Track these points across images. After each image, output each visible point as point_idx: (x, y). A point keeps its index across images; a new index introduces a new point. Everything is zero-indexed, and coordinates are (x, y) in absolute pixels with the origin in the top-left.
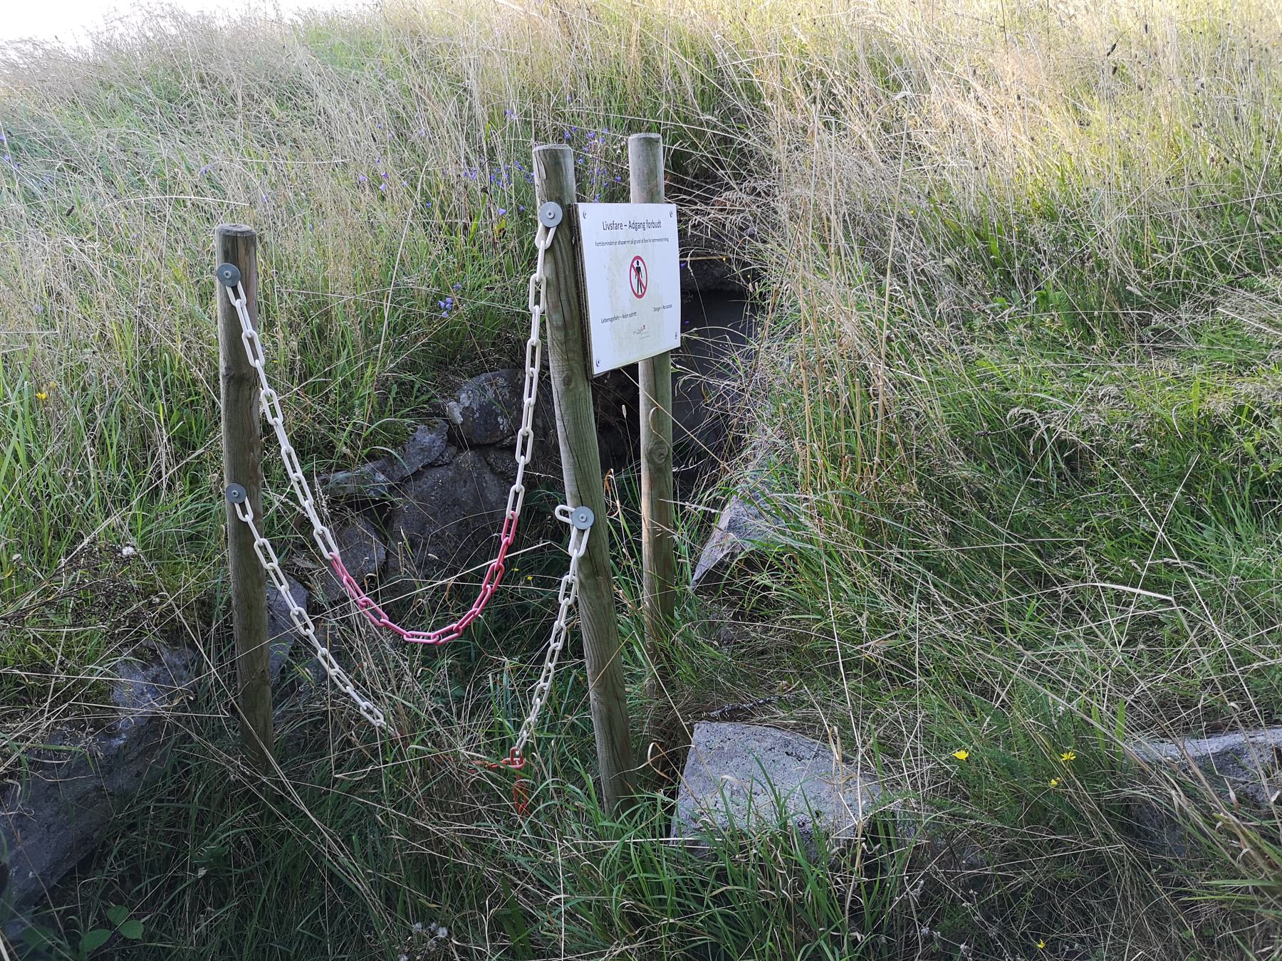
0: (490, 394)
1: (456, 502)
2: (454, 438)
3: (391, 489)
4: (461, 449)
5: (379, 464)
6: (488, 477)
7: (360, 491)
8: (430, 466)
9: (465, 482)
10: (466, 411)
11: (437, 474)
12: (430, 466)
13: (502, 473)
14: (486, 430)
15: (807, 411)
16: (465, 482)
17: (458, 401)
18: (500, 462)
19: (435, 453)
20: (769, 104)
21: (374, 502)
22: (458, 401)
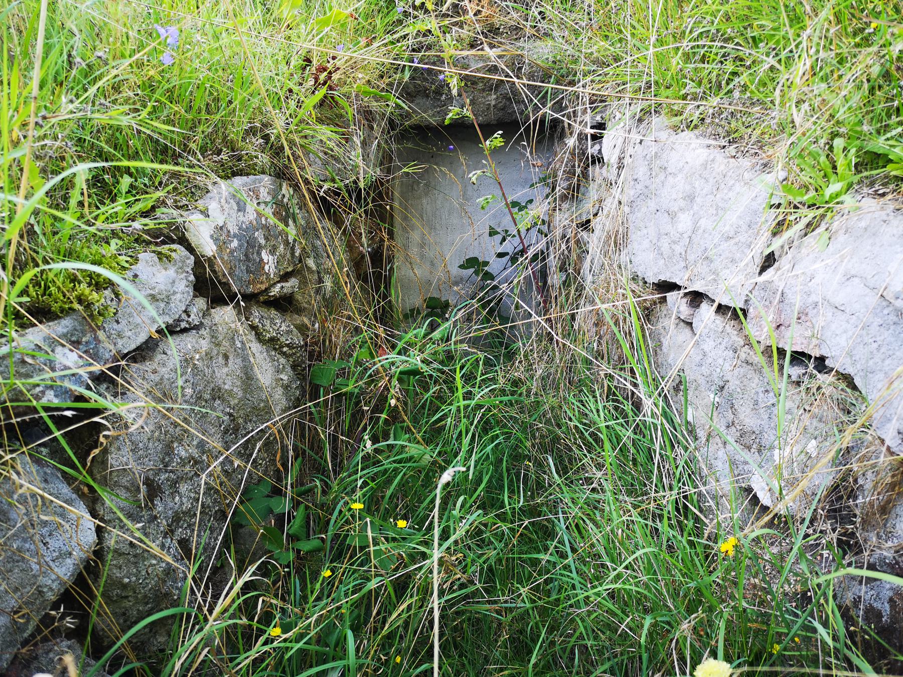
0: (251, 216)
1: (217, 394)
2: (209, 286)
3: (99, 378)
4: (217, 301)
5: (64, 325)
6: (255, 347)
7: (17, 395)
8: (173, 330)
9: (226, 357)
10: (220, 234)
11: (189, 342)
12: (173, 330)
13: (272, 340)
14: (248, 271)
15: (10, 533)
16: (226, 357)
17: (205, 213)
18: (267, 323)
19: (177, 306)
20: (375, 126)
21: (61, 422)
22: (205, 213)
